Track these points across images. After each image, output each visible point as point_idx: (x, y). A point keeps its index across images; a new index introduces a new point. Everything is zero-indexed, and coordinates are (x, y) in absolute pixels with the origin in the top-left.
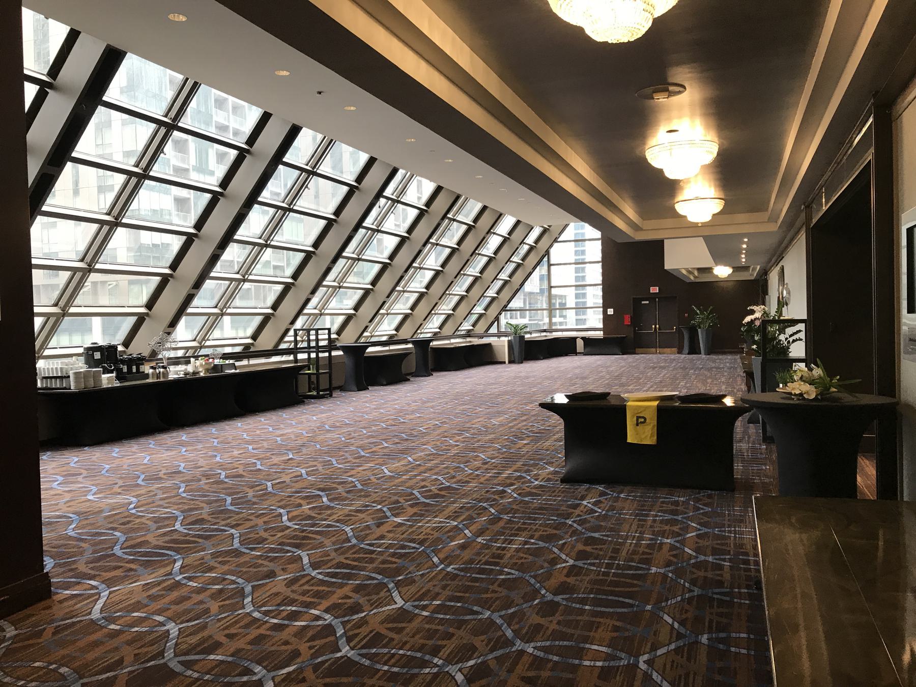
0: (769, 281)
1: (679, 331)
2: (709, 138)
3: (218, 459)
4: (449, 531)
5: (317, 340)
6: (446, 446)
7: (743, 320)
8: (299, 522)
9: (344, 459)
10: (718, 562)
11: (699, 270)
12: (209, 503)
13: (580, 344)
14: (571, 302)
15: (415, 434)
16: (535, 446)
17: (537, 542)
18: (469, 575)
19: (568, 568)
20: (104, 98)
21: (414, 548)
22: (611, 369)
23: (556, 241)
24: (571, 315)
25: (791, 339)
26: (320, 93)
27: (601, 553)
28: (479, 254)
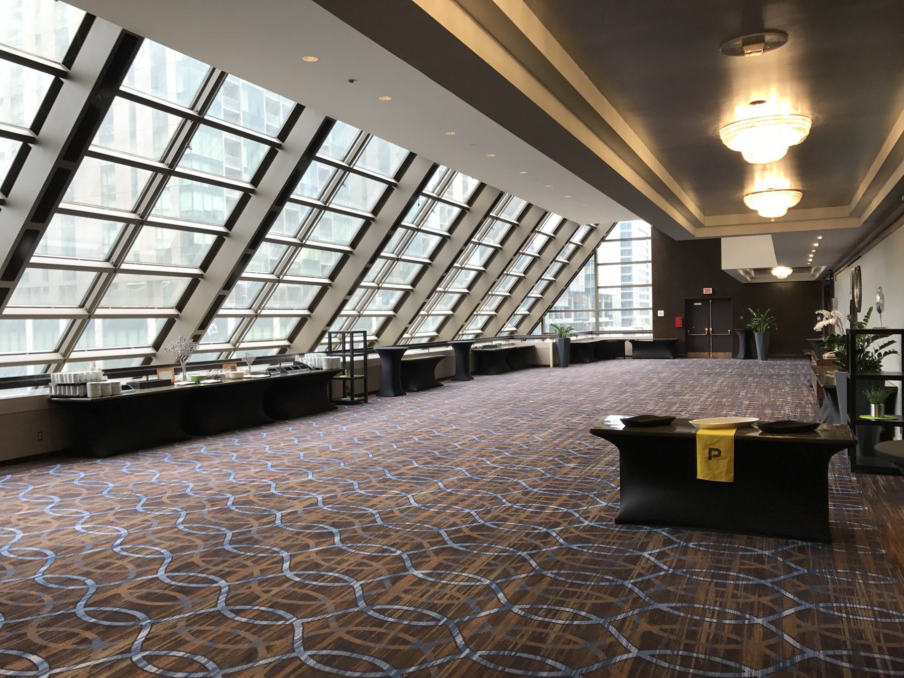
0: (836, 283)
1: (734, 334)
2: (799, 112)
3: (231, 479)
4: (479, 594)
5: (352, 342)
6: (482, 468)
7: (814, 326)
8: (301, 572)
9: (368, 483)
10: (753, 549)
11: (756, 270)
12: (206, 539)
13: (628, 347)
14: (617, 303)
15: (450, 451)
16: (584, 471)
17: (589, 616)
18: (500, 668)
19: (631, 661)
20: (121, 88)
21: (434, 619)
22: (663, 375)
23: (603, 240)
24: (618, 316)
25: (882, 351)
26: (352, 81)
27: (672, 637)
28: (523, 254)
